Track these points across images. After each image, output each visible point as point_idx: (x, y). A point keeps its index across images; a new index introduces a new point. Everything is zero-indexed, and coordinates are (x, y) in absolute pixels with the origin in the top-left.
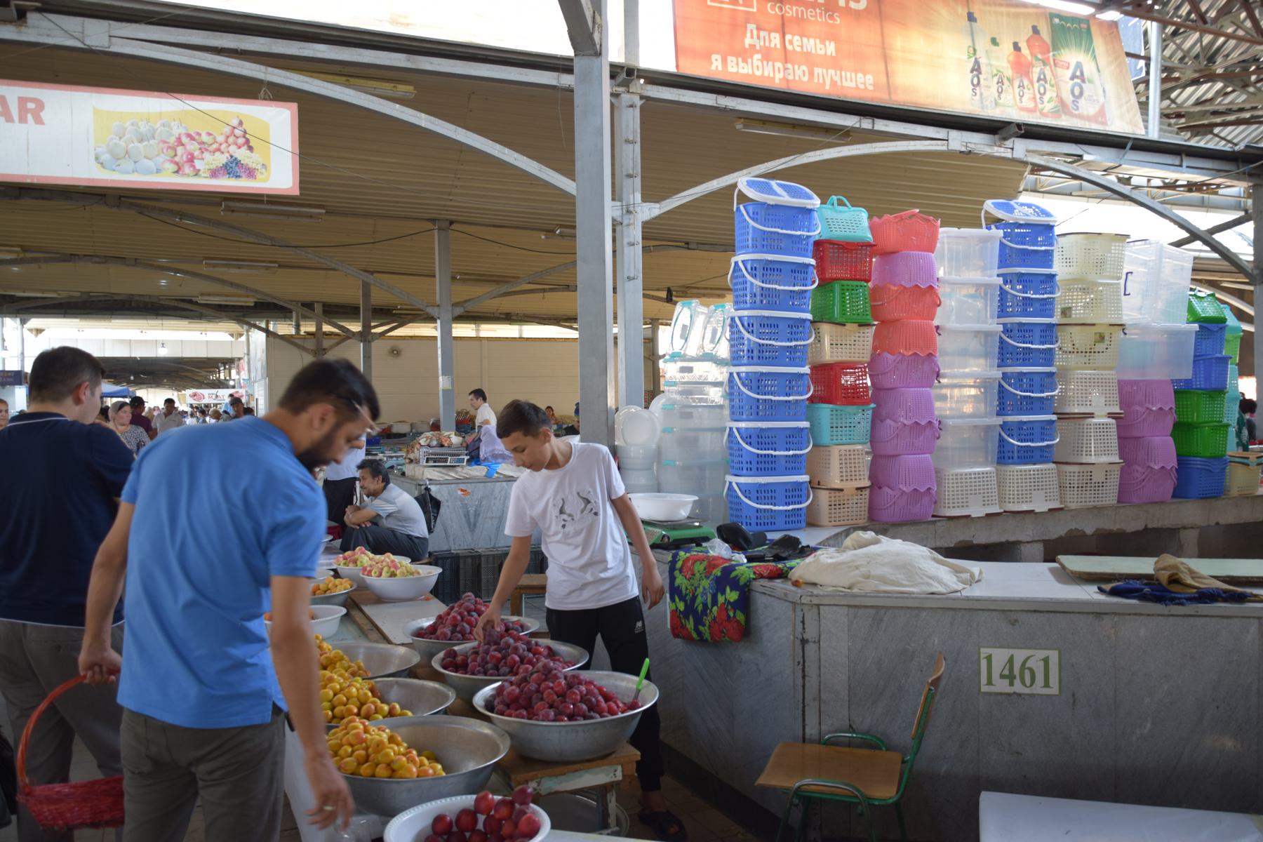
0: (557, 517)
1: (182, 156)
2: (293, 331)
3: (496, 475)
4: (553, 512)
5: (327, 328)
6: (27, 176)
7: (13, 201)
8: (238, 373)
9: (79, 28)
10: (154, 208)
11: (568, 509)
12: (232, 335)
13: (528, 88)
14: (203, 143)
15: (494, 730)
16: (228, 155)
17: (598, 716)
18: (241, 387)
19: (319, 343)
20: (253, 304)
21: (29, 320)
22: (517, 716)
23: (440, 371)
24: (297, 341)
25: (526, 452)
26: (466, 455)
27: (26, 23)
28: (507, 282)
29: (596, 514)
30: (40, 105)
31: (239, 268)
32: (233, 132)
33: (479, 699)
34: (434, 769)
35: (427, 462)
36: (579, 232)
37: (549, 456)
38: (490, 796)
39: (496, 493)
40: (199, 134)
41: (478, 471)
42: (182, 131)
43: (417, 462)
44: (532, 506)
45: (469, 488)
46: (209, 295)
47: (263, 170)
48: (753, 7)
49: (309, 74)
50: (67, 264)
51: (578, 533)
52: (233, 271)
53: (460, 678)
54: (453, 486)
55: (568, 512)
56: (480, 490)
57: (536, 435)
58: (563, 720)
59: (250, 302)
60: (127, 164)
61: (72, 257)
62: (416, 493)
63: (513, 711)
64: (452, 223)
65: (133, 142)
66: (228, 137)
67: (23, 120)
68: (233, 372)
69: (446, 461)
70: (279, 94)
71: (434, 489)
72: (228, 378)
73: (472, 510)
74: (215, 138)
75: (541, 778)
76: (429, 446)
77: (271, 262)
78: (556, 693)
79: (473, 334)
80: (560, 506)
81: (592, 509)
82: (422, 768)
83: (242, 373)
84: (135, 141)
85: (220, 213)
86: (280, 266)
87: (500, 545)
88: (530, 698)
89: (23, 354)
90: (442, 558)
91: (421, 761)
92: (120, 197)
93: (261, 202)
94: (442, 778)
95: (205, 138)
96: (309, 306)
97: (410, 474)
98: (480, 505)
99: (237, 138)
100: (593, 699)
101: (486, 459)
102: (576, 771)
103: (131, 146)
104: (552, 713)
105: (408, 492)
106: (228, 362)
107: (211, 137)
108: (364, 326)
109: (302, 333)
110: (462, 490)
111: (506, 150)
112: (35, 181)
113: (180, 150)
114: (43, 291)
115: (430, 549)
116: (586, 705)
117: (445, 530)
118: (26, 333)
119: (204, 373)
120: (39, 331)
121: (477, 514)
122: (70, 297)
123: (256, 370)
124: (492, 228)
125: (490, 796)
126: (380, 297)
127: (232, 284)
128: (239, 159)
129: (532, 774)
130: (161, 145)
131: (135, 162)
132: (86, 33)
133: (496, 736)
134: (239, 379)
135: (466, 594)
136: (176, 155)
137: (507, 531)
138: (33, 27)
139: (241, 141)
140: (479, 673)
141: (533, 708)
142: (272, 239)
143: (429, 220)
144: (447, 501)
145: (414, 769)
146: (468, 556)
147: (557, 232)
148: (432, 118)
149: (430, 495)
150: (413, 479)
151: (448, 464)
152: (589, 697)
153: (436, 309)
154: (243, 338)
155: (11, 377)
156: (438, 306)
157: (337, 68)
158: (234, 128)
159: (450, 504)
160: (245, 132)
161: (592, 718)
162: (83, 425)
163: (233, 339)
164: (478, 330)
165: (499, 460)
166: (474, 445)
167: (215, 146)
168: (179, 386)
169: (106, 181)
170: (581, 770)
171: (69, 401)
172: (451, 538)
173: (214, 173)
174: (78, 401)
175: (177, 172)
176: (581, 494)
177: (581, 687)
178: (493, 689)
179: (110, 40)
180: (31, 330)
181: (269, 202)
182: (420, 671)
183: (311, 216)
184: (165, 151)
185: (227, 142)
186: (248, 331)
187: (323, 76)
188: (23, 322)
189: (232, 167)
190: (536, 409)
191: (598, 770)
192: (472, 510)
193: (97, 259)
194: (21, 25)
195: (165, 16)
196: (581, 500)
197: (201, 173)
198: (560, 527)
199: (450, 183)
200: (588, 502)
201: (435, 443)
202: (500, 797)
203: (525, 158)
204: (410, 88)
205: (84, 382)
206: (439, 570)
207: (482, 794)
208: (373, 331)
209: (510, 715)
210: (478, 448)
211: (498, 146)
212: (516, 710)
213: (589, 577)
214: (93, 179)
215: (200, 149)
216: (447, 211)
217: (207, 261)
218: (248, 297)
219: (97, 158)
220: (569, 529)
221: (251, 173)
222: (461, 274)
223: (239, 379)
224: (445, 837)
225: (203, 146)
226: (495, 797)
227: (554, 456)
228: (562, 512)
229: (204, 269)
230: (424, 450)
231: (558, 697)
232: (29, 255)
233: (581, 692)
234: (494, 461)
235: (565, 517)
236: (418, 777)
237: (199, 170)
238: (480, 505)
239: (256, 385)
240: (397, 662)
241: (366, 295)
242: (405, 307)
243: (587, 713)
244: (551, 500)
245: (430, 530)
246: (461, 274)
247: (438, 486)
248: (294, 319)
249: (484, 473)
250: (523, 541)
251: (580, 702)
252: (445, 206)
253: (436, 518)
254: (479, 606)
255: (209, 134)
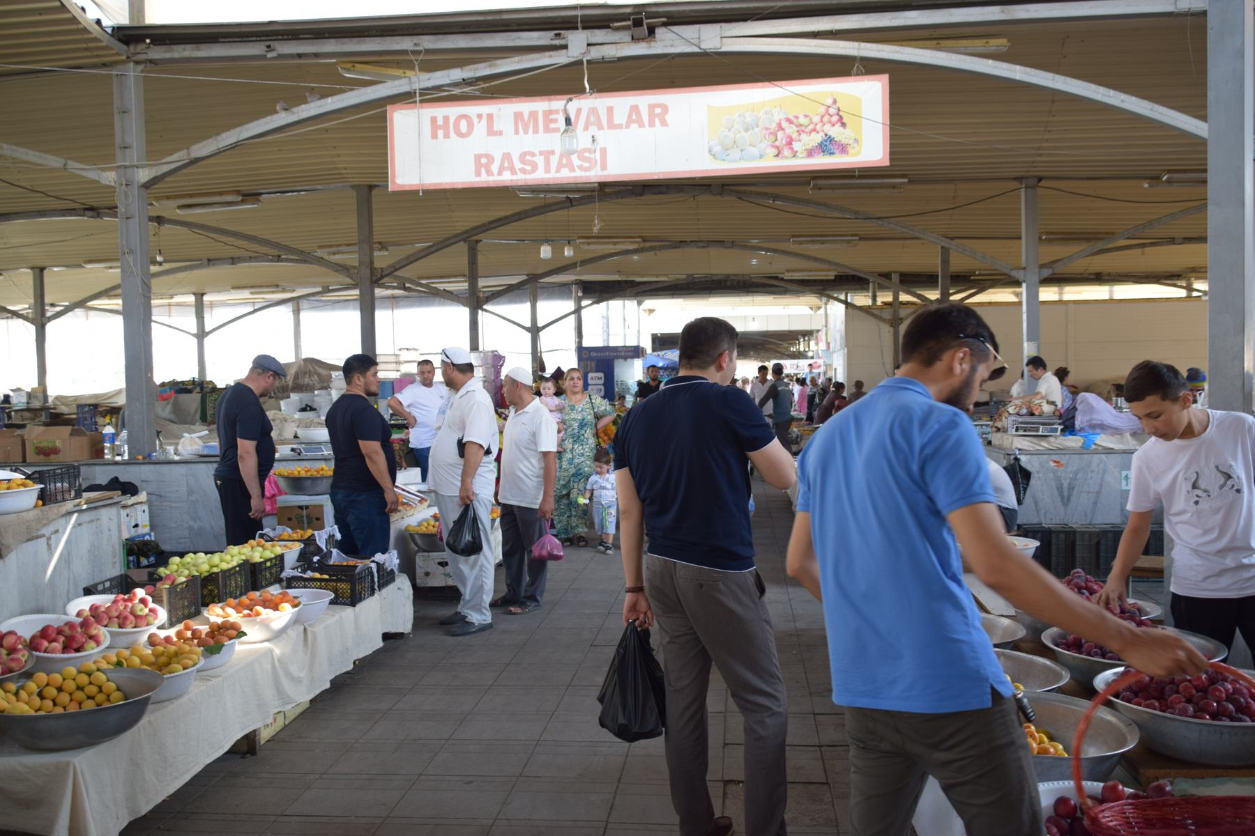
0: (1188, 492)
1: (782, 140)
2: (869, 302)
3: (1094, 447)
4: (1184, 487)
5: (904, 297)
6: (655, 174)
7: (639, 198)
8: (817, 344)
9: (696, 35)
10: (751, 193)
11: (1202, 484)
12: (811, 308)
13: (1128, 20)
14: (801, 125)
15: (1119, 719)
16: (822, 134)
17: (1248, 719)
18: (819, 358)
19: (896, 313)
20: (833, 278)
21: (643, 301)
22: (1147, 706)
23: (1025, 337)
24: (874, 312)
25: (1160, 419)
26: (1059, 424)
27: (654, 37)
28: (1101, 239)
29: (1238, 491)
30: (665, 109)
31: (822, 243)
32: (827, 111)
33: (1102, 680)
34: (1055, 748)
35: (1017, 430)
36: (1210, 175)
37: (1185, 423)
38: (1120, 787)
39: (1094, 465)
40: (797, 117)
41: (1073, 442)
42: (782, 116)
43: (1005, 430)
44: (1157, 479)
45: (1063, 459)
46: (794, 271)
47: (856, 145)
48: (647, 24)
49: (900, 43)
50: (677, 250)
51: (1217, 511)
52: (817, 246)
53: (1074, 658)
54: (1045, 457)
55: (1202, 487)
56: (1074, 463)
57: (1175, 399)
58: (1204, 718)
59: (831, 275)
60: (735, 153)
61: (681, 244)
62: (1005, 463)
63: (1142, 701)
64: (1040, 179)
65: (740, 132)
66: (823, 117)
67: (652, 124)
68: (812, 343)
69: (1037, 431)
70: (870, 67)
71: (1024, 459)
72: (807, 349)
73: (1065, 484)
74: (811, 119)
75: (1175, 778)
76: (1018, 414)
77: (852, 235)
78: (1196, 688)
79: (1055, 298)
80: (1193, 480)
81: (1233, 486)
82: (1042, 745)
83: (820, 344)
84: (742, 130)
85: (809, 192)
86: (862, 239)
87: (1097, 522)
88: (1163, 689)
89: (639, 331)
90: (1055, 532)
91: (1040, 737)
92: (723, 185)
93: (853, 177)
94: (1063, 759)
95: (802, 120)
96: (887, 276)
97: (997, 443)
98: (1075, 478)
99: (832, 116)
100: (1242, 700)
101: (1082, 429)
102: (1217, 776)
103: (738, 136)
104: (1191, 709)
105: (995, 461)
106: (808, 334)
107: (808, 118)
108: (942, 294)
109: (879, 303)
110: (1055, 462)
111: (1112, 92)
112: (661, 177)
113: (780, 134)
114: (657, 276)
115: (1019, 521)
116: (1233, 705)
117: (1035, 503)
118: (642, 312)
119: (786, 345)
120: (651, 311)
121: (1071, 488)
122: (678, 279)
123: (835, 341)
124: (1085, 182)
125: (1120, 787)
126: (959, 263)
127: (816, 259)
128: (833, 136)
129: (1163, 771)
130: (764, 132)
131: (742, 151)
132: (702, 38)
133: (1121, 725)
134: (817, 351)
135: (1075, 570)
136: (776, 140)
137: (1129, 507)
138: (660, 41)
139: (835, 119)
140: (1096, 655)
141: (1166, 700)
142: (856, 213)
143: (1016, 179)
144: (1038, 472)
145: (1035, 745)
146: (1061, 532)
147: (1164, 179)
148: (1028, 69)
149: (1020, 466)
150: (1000, 448)
151: (1040, 433)
152: (1236, 696)
153: (1021, 272)
154: (822, 311)
155: (631, 351)
156: (1024, 268)
157: (927, 33)
158: (829, 107)
159: (1041, 475)
160: (839, 110)
161: (1241, 720)
162: (721, 386)
163: (812, 312)
164: (1061, 294)
165: (1098, 431)
166: (1068, 415)
167: (811, 127)
168: (763, 357)
169: (717, 170)
170: (1223, 776)
171: (712, 369)
172: (1042, 512)
173: (810, 153)
174: (720, 368)
175: (777, 156)
176: (1220, 468)
177: (1226, 684)
178: (1115, 673)
179: (721, 42)
180: (645, 310)
181: (860, 177)
182: (1023, 645)
183: (893, 186)
184: (767, 137)
185: (822, 121)
186: (826, 304)
187: (921, 43)
188: (639, 303)
189: (827, 145)
190: (1173, 371)
191: (1245, 779)
192: (1065, 484)
193: (701, 244)
194: (651, 41)
195: (770, 11)
196: (1219, 475)
197: (798, 154)
198: (1192, 503)
199: (1040, 137)
200: (1229, 477)
201: (1024, 411)
202: (1131, 791)
203: (1134, 98)
204: (1003, 41)
205: (725, 351)
206: (1036, 543)
207: (1110, 783)
208: (952, 298)
209: (1139, 705)
210: (1073, 417)
211: (1102, 90)
212: (1146, 700)
213: (1229, 562)
214: (707, 170)
215: (798, 131)
216: (1035, 167)
217: (795, 239)
218: (829, 270)
219: (710, 151)
220: (1204, 505)
221: (844, 149)
222: (1047, 233)
223: (817, 351)
224: (1069, 821)
225: (800, 128)
226: (1126, 789)
227: (1190, 425)
228: (1195, 486)
229: (792, 247)
230: (1013, 418)
231: (1197, 692)
232: (648, 245)
233: (1227, 690)
234: (1091, 432)
235: (1199, 492)
236: (1038, 753)
237: (797, 152)
238: (1075, 478)
239: (835, 355)
240: (1000, 632)
241: (945, 262)
242: (983, 272)
243: (1234, 714)
244: (1183, 472)
245: (1019, 502)
246: (1047, 233)
247: (1028, 456)
248: (871, 290)
249: (1080, 444)
250: (1143, 516)
251: (1226, 701)
252: (1033, 162)
253: (1025, 489)
254: (1090, 584)
255: (806, 116)
